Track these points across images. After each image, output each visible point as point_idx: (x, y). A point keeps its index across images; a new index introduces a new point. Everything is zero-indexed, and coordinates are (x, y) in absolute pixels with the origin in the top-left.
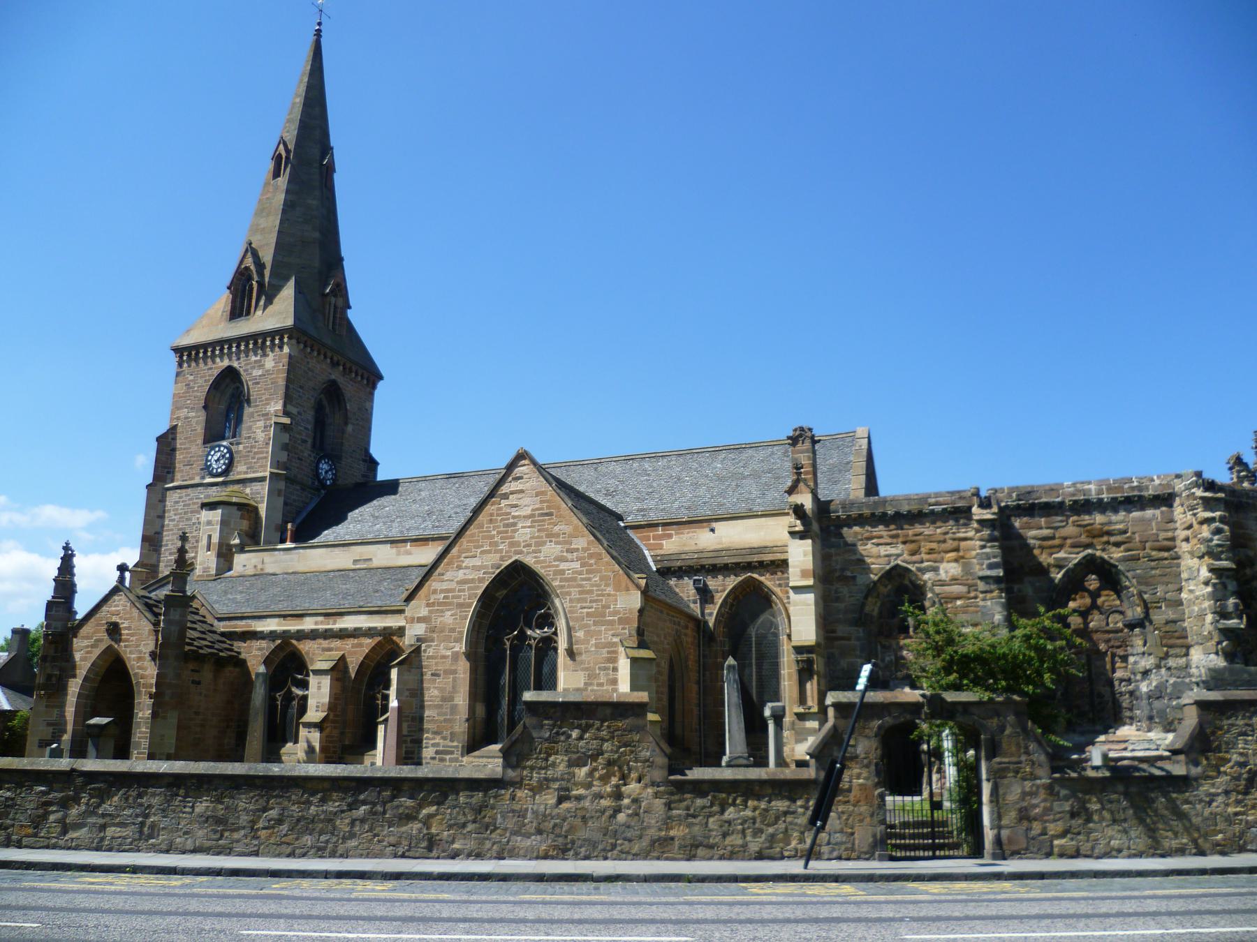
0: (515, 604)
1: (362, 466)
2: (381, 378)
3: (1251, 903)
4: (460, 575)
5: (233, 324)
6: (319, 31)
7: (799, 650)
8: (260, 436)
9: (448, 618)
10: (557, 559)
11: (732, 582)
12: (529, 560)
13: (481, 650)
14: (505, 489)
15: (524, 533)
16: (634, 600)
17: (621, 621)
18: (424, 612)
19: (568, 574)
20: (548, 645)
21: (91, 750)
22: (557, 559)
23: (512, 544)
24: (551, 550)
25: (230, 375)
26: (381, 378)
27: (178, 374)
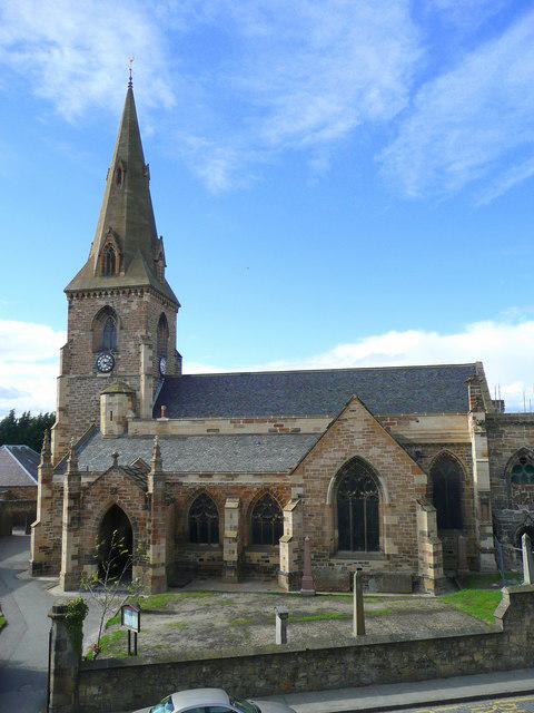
0: (356, 480)
1: (174, 359)
2: (179, 306)
3: (527, 684)
4: (322, 462)
5: (105, 280)
6: (131, 83)
7: (480, 493)
8: (387, 460)
9: (317, 484)
10: (380, 456)
11: (438, 452)
12: (362, 455)
13: (335, 502)
14: (345, 416)
15: (359, 442)
16: (423, 479)
17: (417, 490)
18: (302, 481)
19: (386, 464)
20: (374, 501)
21: (272, 561)
22: (380, 456)
23: (352, 447)
24: (375, 451)
25: (107, 310)
26: (179, 306)
27: (70, 308)
